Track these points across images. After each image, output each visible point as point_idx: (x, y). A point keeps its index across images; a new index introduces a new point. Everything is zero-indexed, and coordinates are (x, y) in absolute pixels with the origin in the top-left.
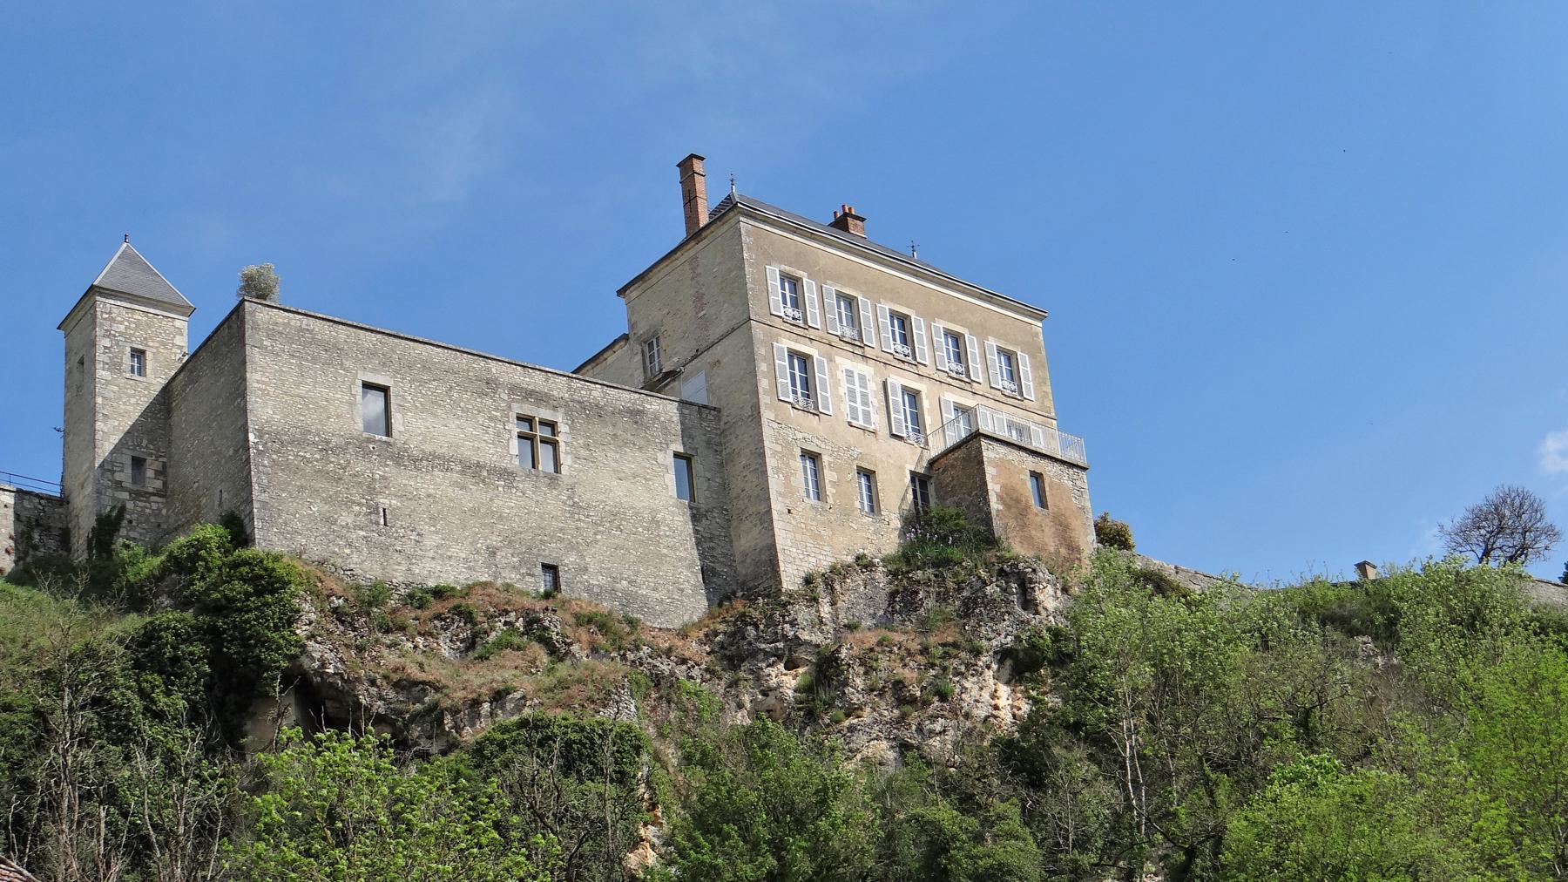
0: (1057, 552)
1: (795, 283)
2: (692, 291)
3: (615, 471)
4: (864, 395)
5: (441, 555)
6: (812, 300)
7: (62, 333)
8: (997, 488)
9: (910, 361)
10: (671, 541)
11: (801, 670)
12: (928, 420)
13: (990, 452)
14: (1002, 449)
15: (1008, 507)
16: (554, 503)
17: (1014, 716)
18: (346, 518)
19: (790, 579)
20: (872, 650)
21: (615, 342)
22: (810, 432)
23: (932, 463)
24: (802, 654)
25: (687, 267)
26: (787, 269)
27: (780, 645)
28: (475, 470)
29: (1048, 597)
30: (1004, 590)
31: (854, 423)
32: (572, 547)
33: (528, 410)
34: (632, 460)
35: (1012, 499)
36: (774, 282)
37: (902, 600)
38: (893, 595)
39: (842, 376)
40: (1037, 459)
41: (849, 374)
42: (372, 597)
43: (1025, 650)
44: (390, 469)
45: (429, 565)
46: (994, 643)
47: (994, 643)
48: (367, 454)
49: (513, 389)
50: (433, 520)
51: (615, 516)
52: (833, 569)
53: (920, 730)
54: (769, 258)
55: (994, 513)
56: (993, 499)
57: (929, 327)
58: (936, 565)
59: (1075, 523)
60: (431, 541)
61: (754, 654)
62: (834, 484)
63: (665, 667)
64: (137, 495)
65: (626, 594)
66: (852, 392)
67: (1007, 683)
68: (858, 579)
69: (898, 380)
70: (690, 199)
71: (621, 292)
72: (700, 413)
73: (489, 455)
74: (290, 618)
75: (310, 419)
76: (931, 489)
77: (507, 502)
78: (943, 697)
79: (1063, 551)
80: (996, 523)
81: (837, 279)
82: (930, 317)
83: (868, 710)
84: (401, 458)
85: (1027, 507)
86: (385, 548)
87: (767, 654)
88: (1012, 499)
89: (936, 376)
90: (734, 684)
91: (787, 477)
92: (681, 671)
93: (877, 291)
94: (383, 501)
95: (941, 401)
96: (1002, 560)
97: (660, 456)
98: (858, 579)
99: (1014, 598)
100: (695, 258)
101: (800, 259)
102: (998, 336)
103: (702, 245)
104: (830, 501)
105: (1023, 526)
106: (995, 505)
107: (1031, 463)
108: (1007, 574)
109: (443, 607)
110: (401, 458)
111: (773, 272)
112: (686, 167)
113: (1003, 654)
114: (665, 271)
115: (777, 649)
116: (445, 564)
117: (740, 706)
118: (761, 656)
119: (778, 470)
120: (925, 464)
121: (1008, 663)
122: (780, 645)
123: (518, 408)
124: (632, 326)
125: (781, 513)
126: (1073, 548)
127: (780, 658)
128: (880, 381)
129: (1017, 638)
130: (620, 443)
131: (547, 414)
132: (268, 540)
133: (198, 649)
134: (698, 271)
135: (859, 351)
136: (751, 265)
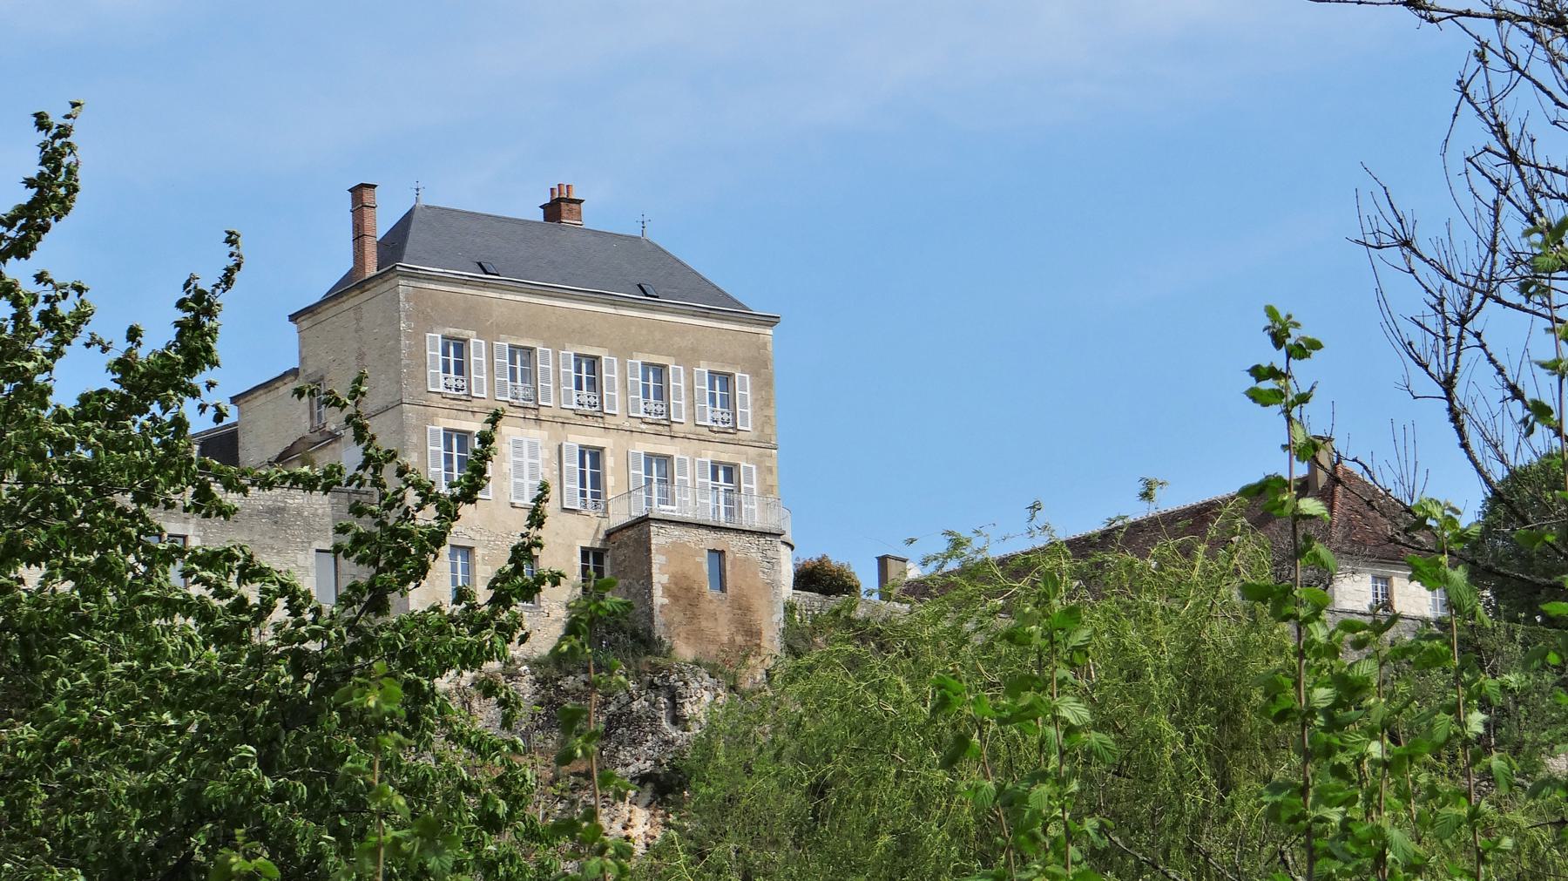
0: (732, 642)
1: (461, 346)
2: (356, 346)
6: (479, 363)
8: (665, 579)
9: (596, 415)
12: (610, 481)
13: (659, 538)
14: (676, 531)
17: (647, 845)
21: (285, 374)
23: (609, 534)
25: (352, 314)
26: (452, 331)
29: (701, 701)
30: (653, 705)
31: (518, 502)
35: (684, 594)
36: (434, 353)
40: (719, 535)
41: (518, 444)
43: (665, 774)
46: (631, 769)
47: (631, 769)
54: (428, 323)
56: (658, 592)
57: (623, 366)
59: (759, 604)
66: (518, 466)
67: (648, 806)
69: (576, 439)
71: (294, 318)
76: (607, 562)
79: (739, 639)
80: (659, 619)
81: (512, 330)
82: (624, 352)
85: (700, 594)
88: (684, 594)
93: (558, 335)
95: (624, 458)
96: (656, 669)
97: (301, 557)
99: (663, 714)
100: (358, 308)
101: (471, 316)
102: (710, 359)
103: (367, 295)
105: (693, 618)
106: (659, 598)
107: (711, 540)
108: (657, 687)
111: (434, 339)
112: (359, 192)
113: (643, 779)
114: (331, 312)
120: (601, 536)
121: (649, 786)
124: (302, 360)
126: (753, 633)
128: (555, 445)
129: (658, 762)
134: (362, 324)
135: (531, 415)
136: (408, 337)
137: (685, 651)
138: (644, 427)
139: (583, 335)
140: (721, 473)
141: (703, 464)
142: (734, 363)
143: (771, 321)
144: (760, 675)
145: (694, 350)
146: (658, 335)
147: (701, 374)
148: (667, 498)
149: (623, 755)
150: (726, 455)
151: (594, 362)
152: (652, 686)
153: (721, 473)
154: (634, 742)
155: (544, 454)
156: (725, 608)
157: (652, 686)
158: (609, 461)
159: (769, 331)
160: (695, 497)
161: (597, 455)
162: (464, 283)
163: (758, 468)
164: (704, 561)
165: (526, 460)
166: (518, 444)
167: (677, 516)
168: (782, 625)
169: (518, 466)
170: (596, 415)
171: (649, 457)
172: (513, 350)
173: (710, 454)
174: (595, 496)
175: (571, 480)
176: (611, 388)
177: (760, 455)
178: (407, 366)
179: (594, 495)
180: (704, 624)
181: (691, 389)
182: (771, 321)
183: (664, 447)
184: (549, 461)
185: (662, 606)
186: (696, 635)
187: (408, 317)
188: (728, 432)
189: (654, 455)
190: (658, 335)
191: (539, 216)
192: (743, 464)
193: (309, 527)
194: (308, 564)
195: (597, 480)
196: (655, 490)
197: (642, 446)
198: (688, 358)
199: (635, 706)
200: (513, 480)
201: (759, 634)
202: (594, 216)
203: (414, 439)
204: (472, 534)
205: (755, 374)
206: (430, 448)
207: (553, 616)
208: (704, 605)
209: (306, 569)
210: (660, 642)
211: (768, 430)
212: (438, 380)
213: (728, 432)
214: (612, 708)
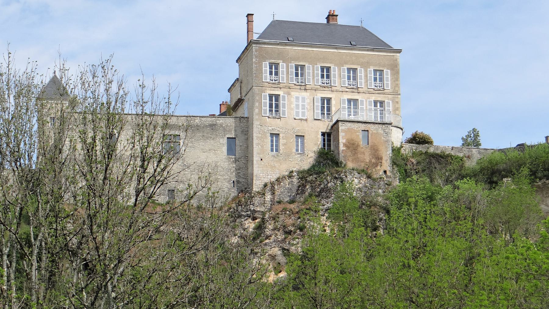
0: (370, 161)
3: (202, 149)
4: (303, 105)
10: (222, 173)
11: (257, 221)
19: (257, 186)
20: (278, 214)
21: (235, 82)
22: (274, 125)
24: (257, 215)
26: (273, 61)
27: (249, 213)
30: (335, 184)
31: (297, 118)
34: (210, 144)
36: (266, 68)
37: (301, 189)
38: (299, 187)
39: (293, 100)
40: (366, 125)
41: (297, 98)
47: (325, 206)
52: (278, 180)
53: (289, 243)
55: (341, 152)
57: (340, 70)
58: (317, 174)
61: (240, 216)
62: (284, 144)
66: (297, 106)
68: (287, 181)
70: (249, 31)
72: (240, 120)
78: (301, 229)
83: (273, 236)
87: (245, 216)
88: (352, 146)
89: (341, 90)
91: (262, 146)
93: (313, 61)
96: (337, 172)
97: (221, 140)
98: (287, 181)
101: (280, 55)
102: (374, 66)
104: (281, 152)
105: (355, 154)
106: (342, 147)
108: (337, 178)
115: (248, 214)
117: (235, 235)
118: (243, 217)
119: (258, 144)
122: (249, 213)
125: (257, 161)
126: (379, 159)
127: (250, 217)
135: (303, 88)
137: (350, 165)
138: (347, 90)
139: (324, 60)
140: (378, 104)
141: (370, 102)
142: (384, 66)
143: (399, 51)
144: (381, 173)
145: (368, 63)
146: (354, 58)
147: (371, 71)
148: (356, 113)
149: (323, 202)
150: (380, 98)
151: (328, 69)
152: (336, 178)
153: (378, 104)
154: (328, 197)
155: (307, 101)
156: (368, 150)
157: (336, 178)
158: (333, 102)
159: (398, 55)
160: (367, 112)
161: (329, 100)
162: (278, 44)
163: (393, 102)
164: (360, 135)
165: (300, 103)
166: (297, 98)
167: (360, 119)
168: (391, 155)
169: (297, 106)
170: (329, 87)
171: (349, 101)
172: (349, 70)
173: (373, 98)
174: (277, 111)
175: (317, 109)
176: (361, 79)
177: (393, 97)
178: (255, 73)
179: (276, 111)
180: (359, 156)
181: (366, 76)
182: (399, 51)
183: (355, 96)
184: (309, 103)
185: (343, 150)
186: (356, 160)
187: (256, 57)
188: (381, 90)
189: (352, 99)
190: (354, 58)
191: (325, 21)
192: (386, 101)
193: (225, 130)
194: (224, 142)
195: (329, 109)
196: (352, 110)
197: (346, 96)
198: (365, 66)
199: (329, 185)
200: (295, 110)
201: (381, 159)
202: (341, 21)
203: (257, 98)
204: (279, 129)
205: (392, 70)
206: (263, 101)
207: (309, 156)
208: (359, 149)
209: (223, 144)
210: (341, 163)
211: (397, 89)
212: (266, 76)
213: (381, 90)
214: (322, 186)
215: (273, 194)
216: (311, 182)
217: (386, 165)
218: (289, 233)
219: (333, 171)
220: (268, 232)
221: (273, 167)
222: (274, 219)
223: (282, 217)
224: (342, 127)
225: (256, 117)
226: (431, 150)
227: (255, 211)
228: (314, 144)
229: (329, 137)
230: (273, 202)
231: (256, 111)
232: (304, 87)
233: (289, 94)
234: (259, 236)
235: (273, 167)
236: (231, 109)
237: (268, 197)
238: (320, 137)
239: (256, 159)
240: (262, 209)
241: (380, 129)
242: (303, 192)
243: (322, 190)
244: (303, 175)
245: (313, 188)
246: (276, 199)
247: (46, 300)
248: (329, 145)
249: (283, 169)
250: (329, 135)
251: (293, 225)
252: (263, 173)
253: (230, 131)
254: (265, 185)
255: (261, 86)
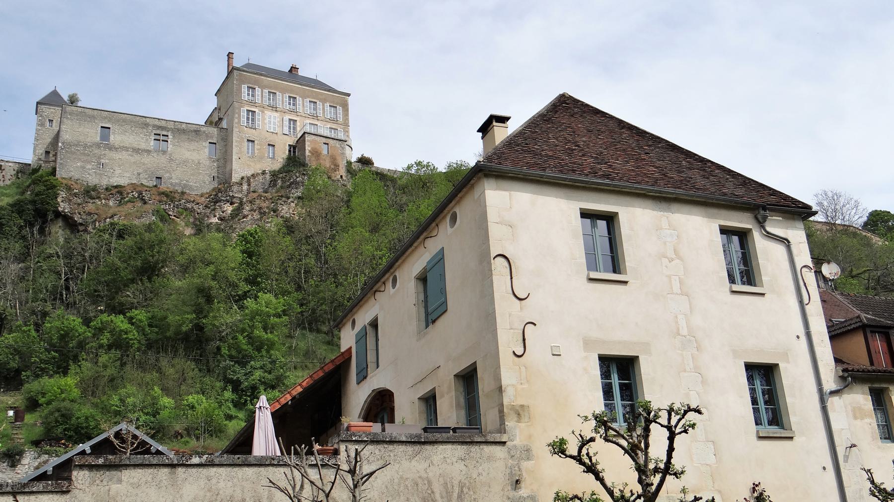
5: (121, 176)
7: (480, 134)
15: (313, 154)
16: (163, 160)
18: (89, 166)
19: (235, 178)
22: (251, 134)
24: (234, 200)
28: (137, 151)
32: (168, 172)
33: (158, 132)
34: (194, 145)
37: (273, 183)
42: (95, 188)
44: (107, 151)
45: (115, 179)
48: (100, 147)
49: (154, 126)
50: (120, 166)
51: (185, 162)
52: (253, 175)
60: (118, 171)
61: (220, 201)
63: (189, 206)
64: (46, 162)
65: (185, 185)
68: (261, 177)
73: (143, 146)
74: (56, 196)
75: (81, 138)
77: (146, 159)
78: (274, 212)
84: (111, 148)
86: (101, 175)
90: (214, 210)
92: (196, 207)
93: (283, 91)
94: (103, 161)
106: (307, 153)
109: (118, 191)
110: (111, 148)
116: (121, 177)
117: (215, 216)
123: (155, 132)
126: (336, 167)
130: (190, 140)
131: (165, 133)
132: (61, 174)
133: (30, 207)
139: (291, 91)
157: (304, 174)
158: (298, 124)
181: (324, 109)
183: (316, 122)
205: (343, 108)
215: (249, 185)
216: (282, 178)
217: (342, 171)
218: (265, 213)
219: (301, 169)
220: (245, 212)
221: (249, 166)
222: (251, 202)
223: (258, 202)
224: (307, 138)
225: (235, 130)
226: (373, 169)
227: (233, 197)
228: (282, 154)
229: (297, 148)
230: (249, 192)
231: (236, 120)
232: (274, 108)
233: (263, 112)
234: (237, 215)
235: (249, 166)
236: (214, 121)
237: (245, 187)
238: (288, 148)
239: (235, 157)
240: (240, 196)
241: (337, 144)
242: (275, 185)
243: (292, 183)
244: (274, 174)
245: (283, 182)
246: (252, 189)
247: (155, 445)
248: (294, 152)
249: (257, 168)
250: (294, 147)
251: (267, 208)
252: (240, 168)
253: (212, 137)
254: (242, 178)
255: (241, 102)
